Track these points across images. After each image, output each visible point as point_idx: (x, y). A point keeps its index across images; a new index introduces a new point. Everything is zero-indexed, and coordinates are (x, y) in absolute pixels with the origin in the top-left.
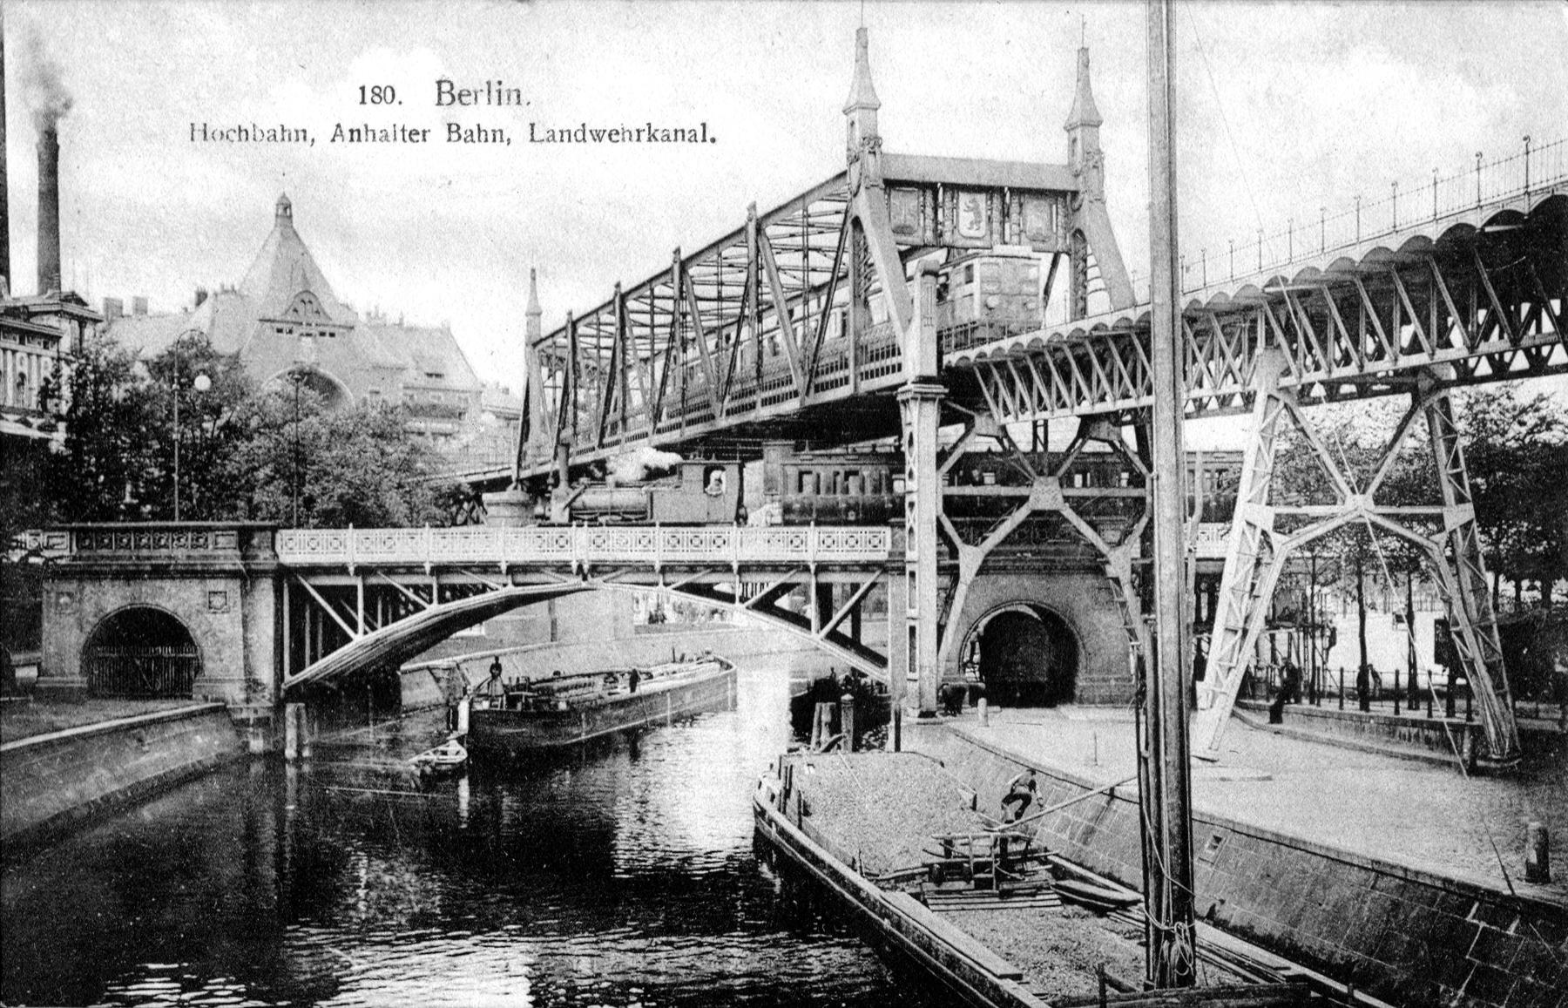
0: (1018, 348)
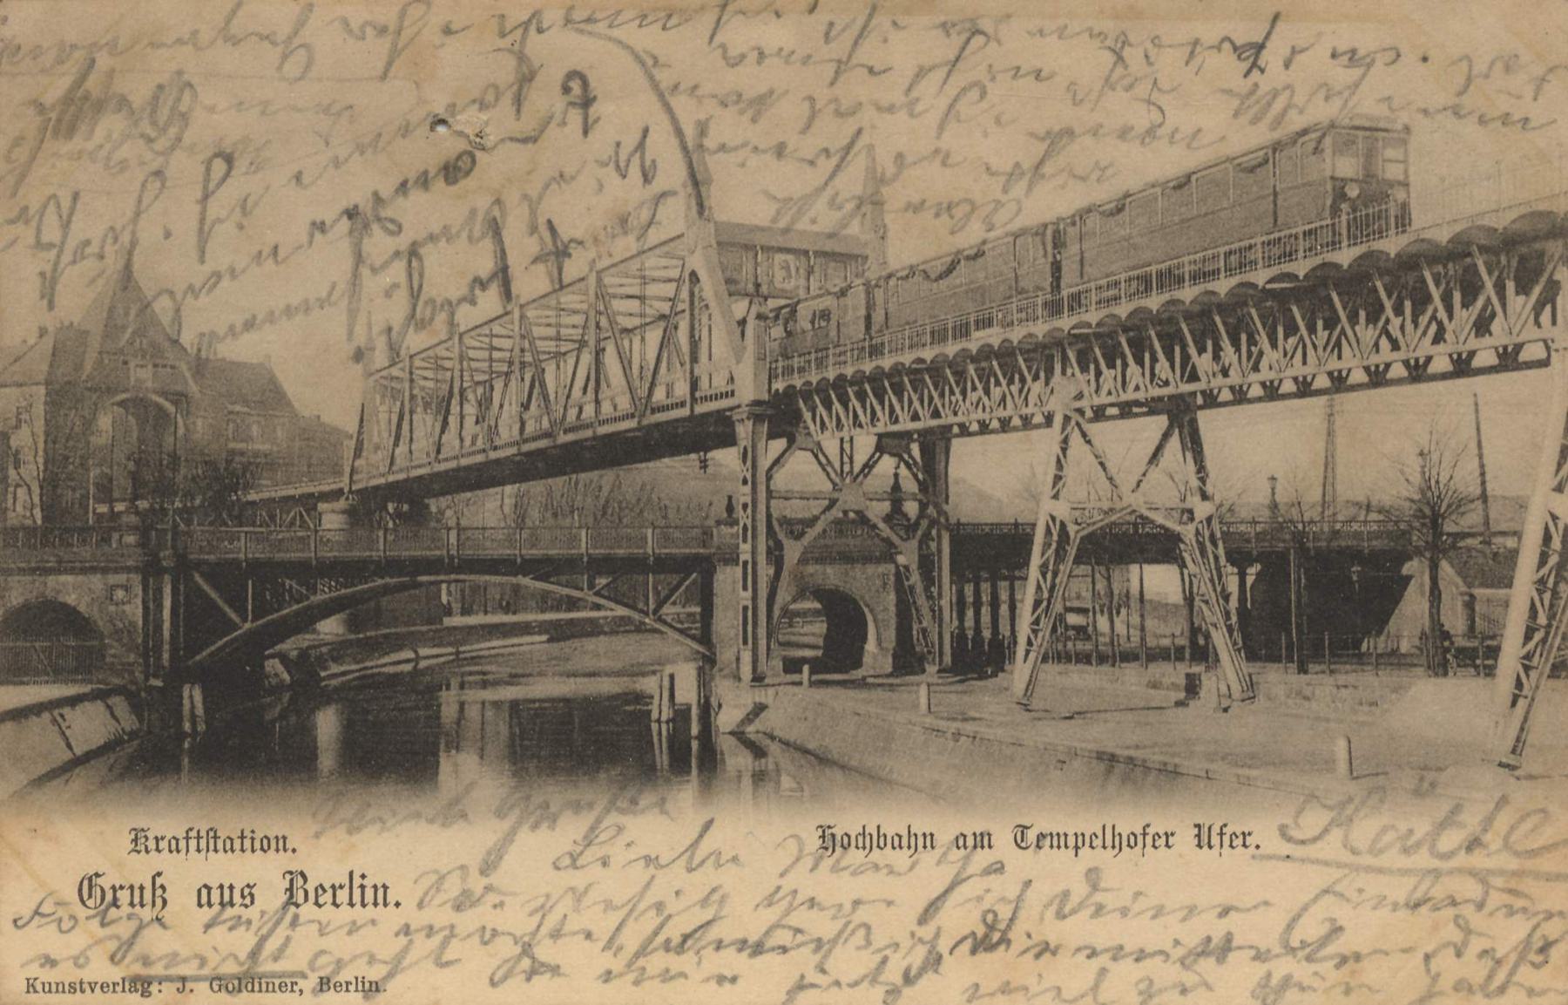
0: (1006, 344)
